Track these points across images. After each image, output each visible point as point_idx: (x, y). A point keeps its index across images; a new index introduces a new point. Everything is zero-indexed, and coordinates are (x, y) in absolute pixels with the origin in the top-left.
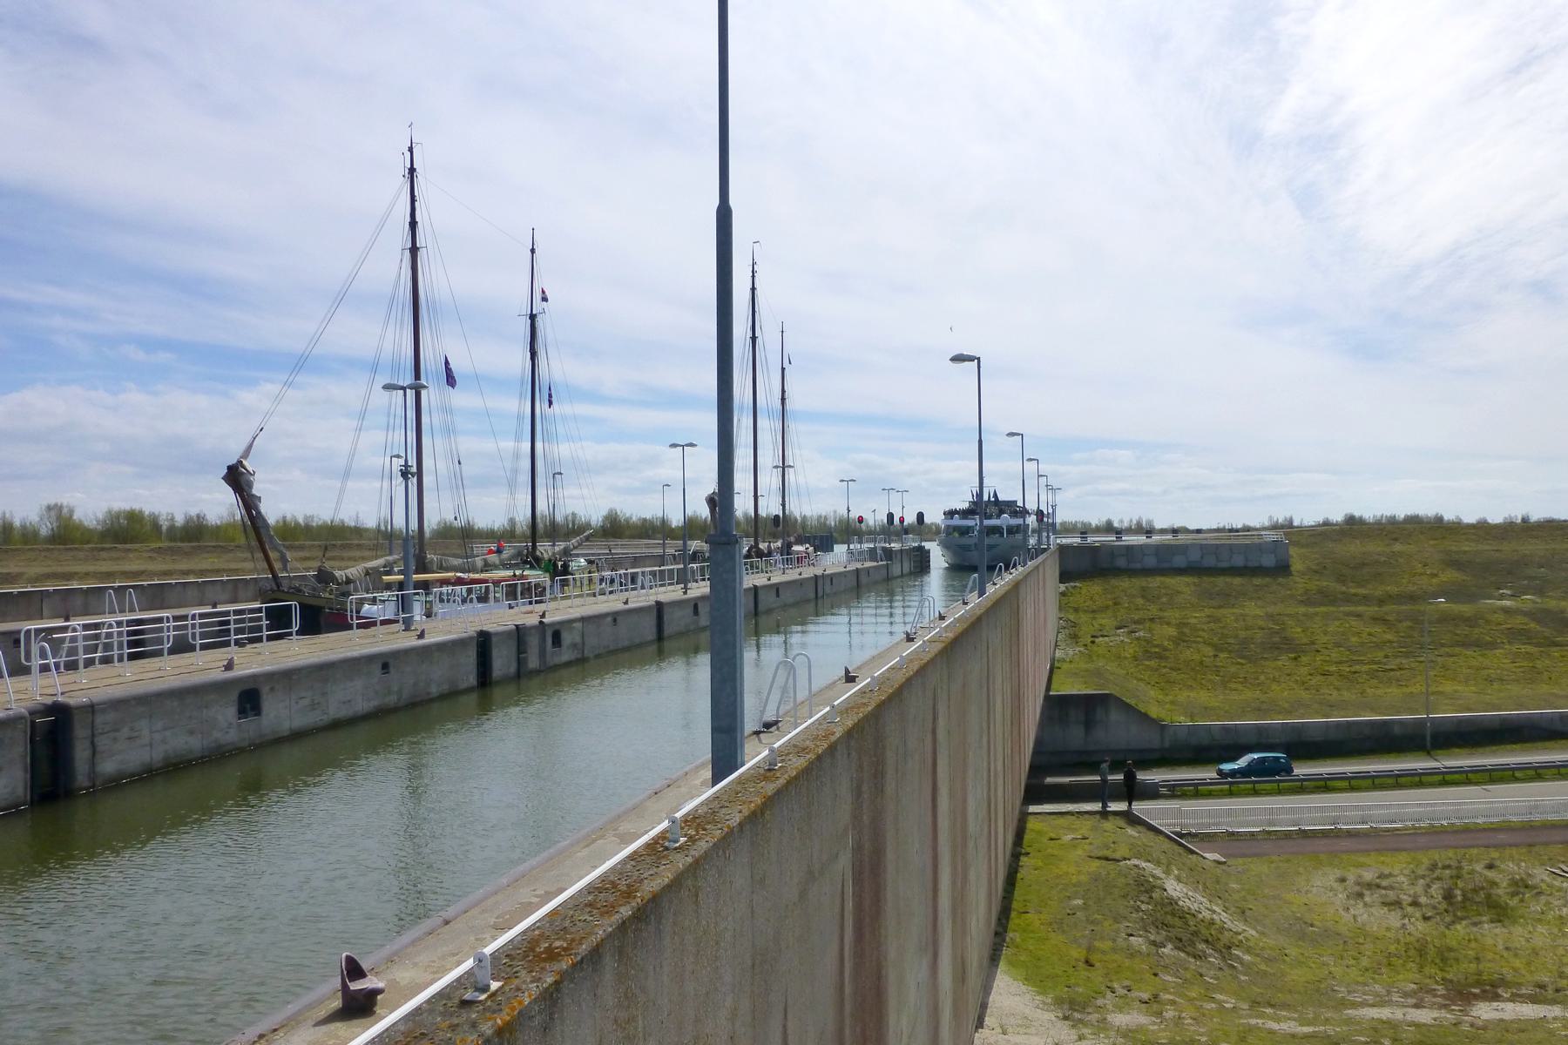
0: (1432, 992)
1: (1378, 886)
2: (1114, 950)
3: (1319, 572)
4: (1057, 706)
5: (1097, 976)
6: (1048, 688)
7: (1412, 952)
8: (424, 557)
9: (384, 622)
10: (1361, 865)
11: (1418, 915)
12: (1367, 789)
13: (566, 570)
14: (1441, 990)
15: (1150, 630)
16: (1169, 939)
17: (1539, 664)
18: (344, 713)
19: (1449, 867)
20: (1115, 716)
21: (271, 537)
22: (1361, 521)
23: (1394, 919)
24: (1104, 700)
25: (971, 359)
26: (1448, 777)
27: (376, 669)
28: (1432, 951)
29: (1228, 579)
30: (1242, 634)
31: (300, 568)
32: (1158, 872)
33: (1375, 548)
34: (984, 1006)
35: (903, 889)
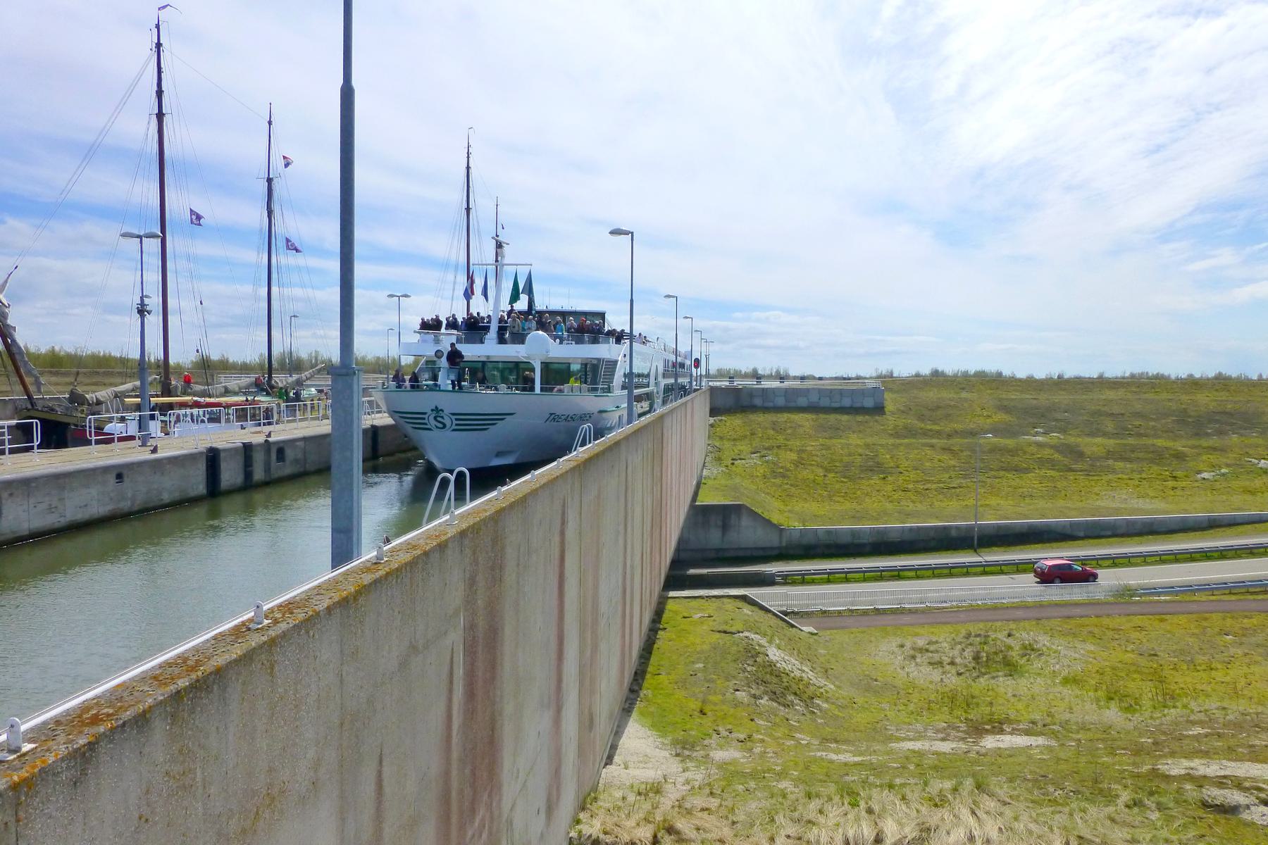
0: (957, 729)
1: (927, 651)
2: (723, 702)
3: (906, 411)
4: (700, 514)
5: (707, 721)
6: (694, 498)
7: (946, 700)
8: (166, 386)
9: (121, 439)
10: (916, 635)
11: (954, 671)
12: (929, 577)
13: (298, 397)
14: (963, 727)
15: (777, 455)
16: (766, 693)
17: (1059, 485)
18: (81, 516)
19: (979, 635)
20: (745, 521)
21: (26, 363)
22: (943, 374)
23: (936, 675)
24: (738, 509)
25: (626, 233)
26: (987, 569)
27: (112, 479)
28: (960, 699)
29: (838, 416)
30: (846, 459)
31: (53, 392)
32: (763, 642)
33: (947, 395)
34: (614, 747)
35: (524, 658)
